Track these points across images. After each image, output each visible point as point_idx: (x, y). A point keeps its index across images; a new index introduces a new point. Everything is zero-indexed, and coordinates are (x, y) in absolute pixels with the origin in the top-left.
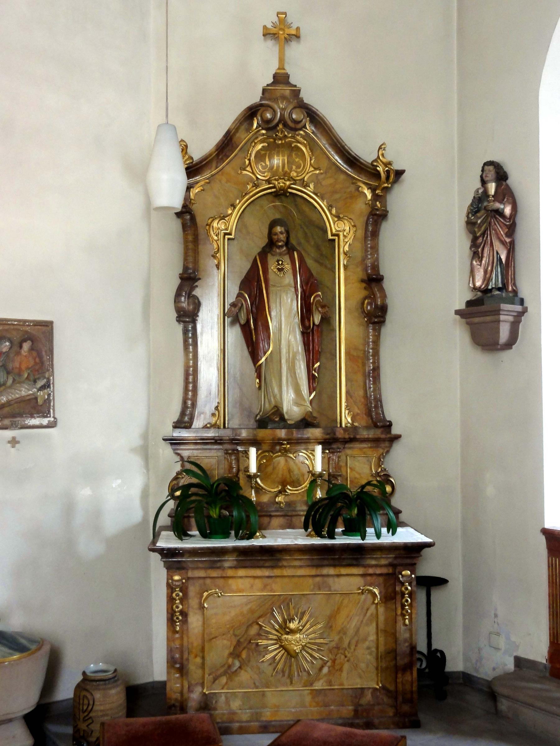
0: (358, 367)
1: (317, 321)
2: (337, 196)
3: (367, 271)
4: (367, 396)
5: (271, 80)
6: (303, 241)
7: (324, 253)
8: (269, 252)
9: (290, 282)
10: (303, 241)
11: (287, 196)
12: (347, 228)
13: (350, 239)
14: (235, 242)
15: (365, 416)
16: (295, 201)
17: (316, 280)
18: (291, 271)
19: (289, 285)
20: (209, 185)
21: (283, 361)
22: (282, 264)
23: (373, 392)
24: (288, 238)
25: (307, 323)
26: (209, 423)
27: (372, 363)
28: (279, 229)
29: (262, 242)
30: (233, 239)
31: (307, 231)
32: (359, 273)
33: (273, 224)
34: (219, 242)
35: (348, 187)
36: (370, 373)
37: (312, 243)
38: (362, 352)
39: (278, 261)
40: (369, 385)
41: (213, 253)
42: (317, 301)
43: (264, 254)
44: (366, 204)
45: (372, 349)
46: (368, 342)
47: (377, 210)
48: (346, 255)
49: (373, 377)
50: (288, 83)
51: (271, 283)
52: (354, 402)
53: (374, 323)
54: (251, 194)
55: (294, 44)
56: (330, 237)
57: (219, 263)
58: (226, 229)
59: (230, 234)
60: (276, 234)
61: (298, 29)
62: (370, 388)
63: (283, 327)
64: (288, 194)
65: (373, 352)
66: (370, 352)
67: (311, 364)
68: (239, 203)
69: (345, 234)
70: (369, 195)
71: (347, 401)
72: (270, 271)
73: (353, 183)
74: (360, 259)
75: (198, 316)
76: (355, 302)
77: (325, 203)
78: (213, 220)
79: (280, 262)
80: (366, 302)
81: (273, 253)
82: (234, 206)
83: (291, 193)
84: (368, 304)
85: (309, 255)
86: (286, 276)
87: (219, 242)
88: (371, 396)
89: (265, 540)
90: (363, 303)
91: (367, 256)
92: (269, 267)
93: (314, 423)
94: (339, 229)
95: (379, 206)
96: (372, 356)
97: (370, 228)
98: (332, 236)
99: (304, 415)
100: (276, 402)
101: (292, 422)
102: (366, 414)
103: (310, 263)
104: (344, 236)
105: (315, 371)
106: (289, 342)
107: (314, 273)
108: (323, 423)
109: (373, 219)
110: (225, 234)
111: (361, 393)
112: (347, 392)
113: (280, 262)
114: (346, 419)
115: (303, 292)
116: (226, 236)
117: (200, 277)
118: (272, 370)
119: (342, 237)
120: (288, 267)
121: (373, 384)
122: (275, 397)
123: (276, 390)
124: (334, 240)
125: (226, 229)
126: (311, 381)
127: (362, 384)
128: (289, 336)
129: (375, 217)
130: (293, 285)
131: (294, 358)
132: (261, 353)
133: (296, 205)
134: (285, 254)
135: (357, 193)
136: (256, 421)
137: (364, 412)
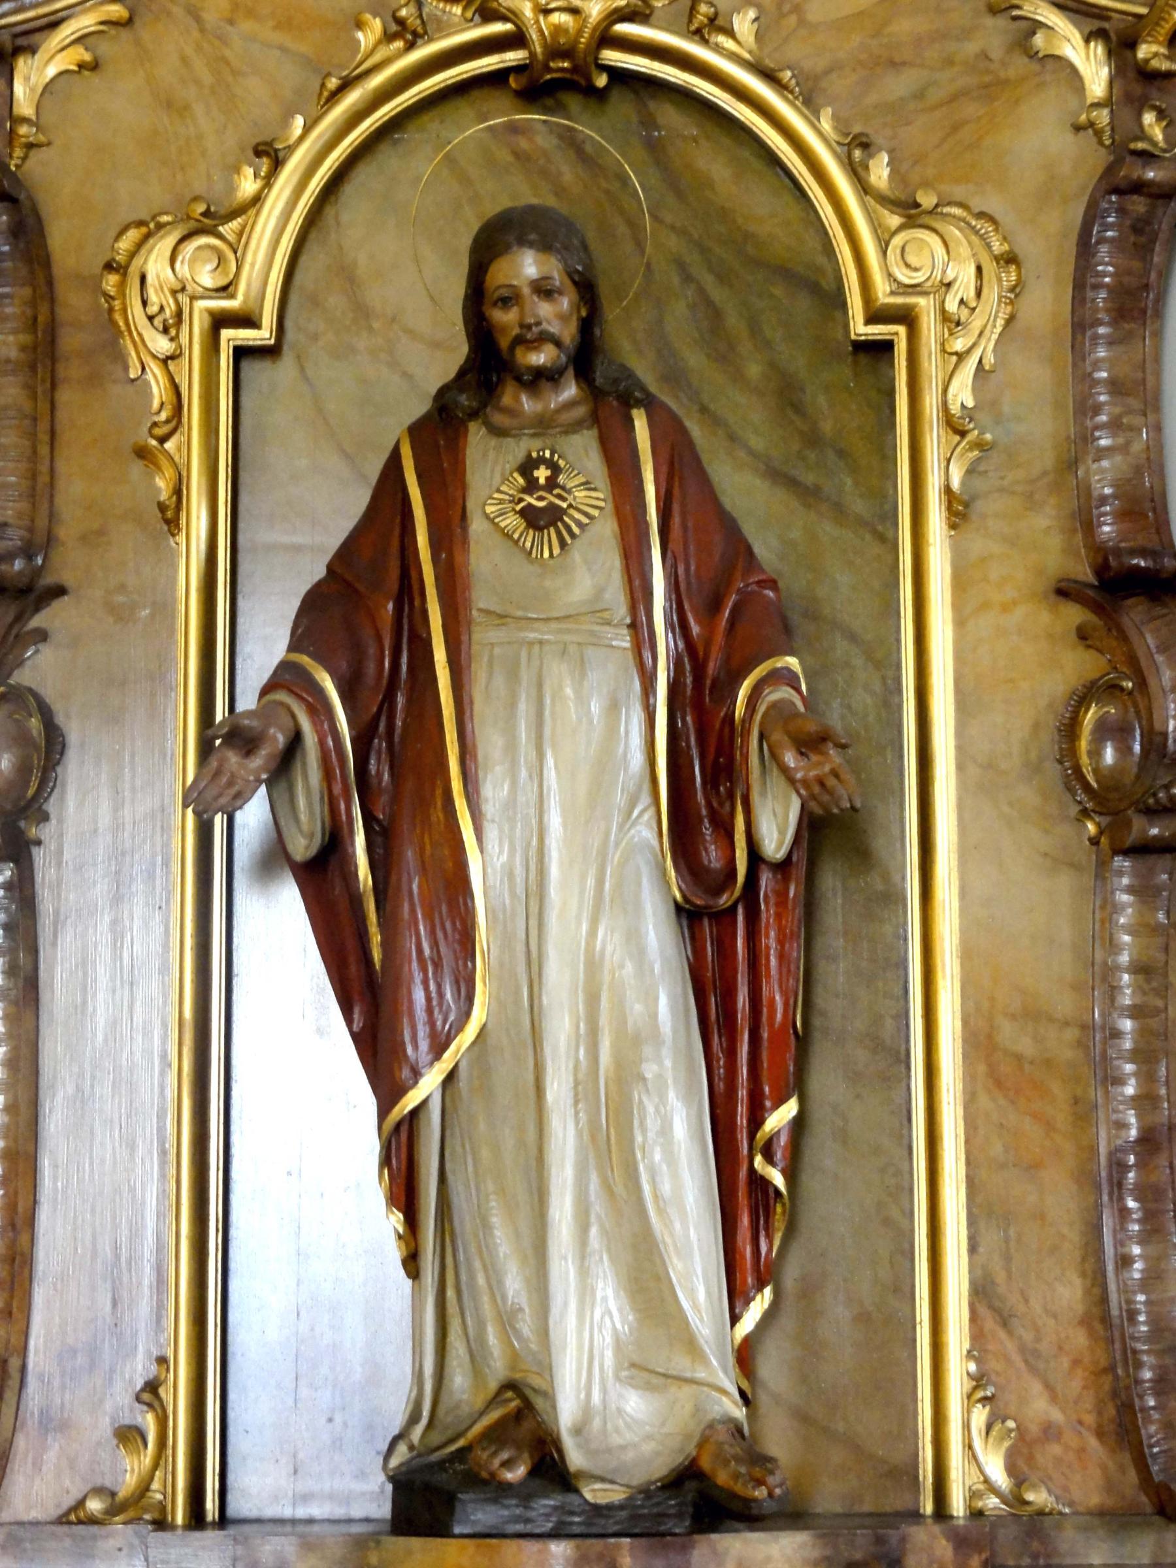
0: (1049, 1126)
1: (775, 838)
2: (898, 86)
3: (1089, 527)
4: (1106, 1319)
6: (694, 359)
7: (827, 427)
8: (474, 414)
9: (600, 591)
10: (694, 359)
11: (591, 92)
12: (964, 276)
13: (982, 336)
14: (285, 370)
15: (1093, 1442)
16: (649, 122)
17: (772, 584)
18: (606, 529)
19: (597, 612)
20: (124, 34)
21: (558, 1090)
22: (552, 484)
23: (1145, 1284)
24: (588, 326)
25: (713, 856)
26: (99, 1491)
27: (1136, 1101)
28: (528, 266)
29: (440, 357)
30: (269, 352)
31: (717, 294)
32: (1045, 544)
33: (489, 245)
34: (180, 370)
35: (966, 34)
36: (1123, 1168)
37: (754, 370)
38: (1071, 1034)
39: (527, 467)
40: (1119, 1243)
42: (774, 706)
43: (441, 431)
44: (1078, 128)
45: (1136, 1012)
46: (1108, 974)
47: (1147, 157)
48: (963, 434)
49: (1140, 1193)
51: (482, 598)
52: (1022, 1349)
53: (1142, 850)
54: (376, 81)
56: (861, 329)
57: (178, 492)
58: (225, 290)
59: (247, 321)
60: (508, 300)
62: (1125, 1261)
63: (554, 871)
64: (602, 81)
65: (1142, 1033)
66: (1116, 1034)
67: (742, 1110)
68: (301, 139)
69: (952, 306)
70: (1094, 71)
71: (978, 1348)
72: (477, 526)
74: (1048, 460)
75: (46, 818)
76: (1023, 718)
77: (826, 125)
78: (147, 237)
79: (542, 474)
80: (1090, 716)
81: (498, 419)
82: (271, 155)
83: (619, 76)
84: (1103, 731)
85: (732, 438)
86: (576, 554)
87: (180, 370)
88: (1132, 1315)
90: (1070, 730)
91: (1085, 438)
92: (471, 505)
93: (748, 1501)
94: (919, 278)
95: (1158, 134)
96: (1136, 1055)
97: (1106, 269)
98: (871, 320)
99: (691, 1449)
100: (514, 1358)
101: (613, 1495)
102: (1100, 1434)
103: (740, 488)
104: (945, 317)
105: (769, 1158)
106: (593, 965)
107: (765, 549)
108: (828, 1498)
109: (1121, 211)
110: (220, 321)
111: (1070, 1293)
112: (982, 1292)
113: (542, 474)
114: (976, 1466)
115: (691, 656)
116: (226, 334)
117: (67, 578)
118: (485, 1153)
119: (930, 326)
120: (586, 491)
121: (1144, 1239)
122: (507, 1320)
123: (514, 1285)
124: (885, 348)
125: (225, 290)
126: (745, 1220)
127: (1073, 1236)
128: (592, 933)
129: (1138, 205)
130: (621, 611)
131: (627, 1076)
132: (418, 1048)
133: (655, 148)
134: (574, 427)
135: (1019, 65)
136: (392, 1479)
137: (1090, 1419)
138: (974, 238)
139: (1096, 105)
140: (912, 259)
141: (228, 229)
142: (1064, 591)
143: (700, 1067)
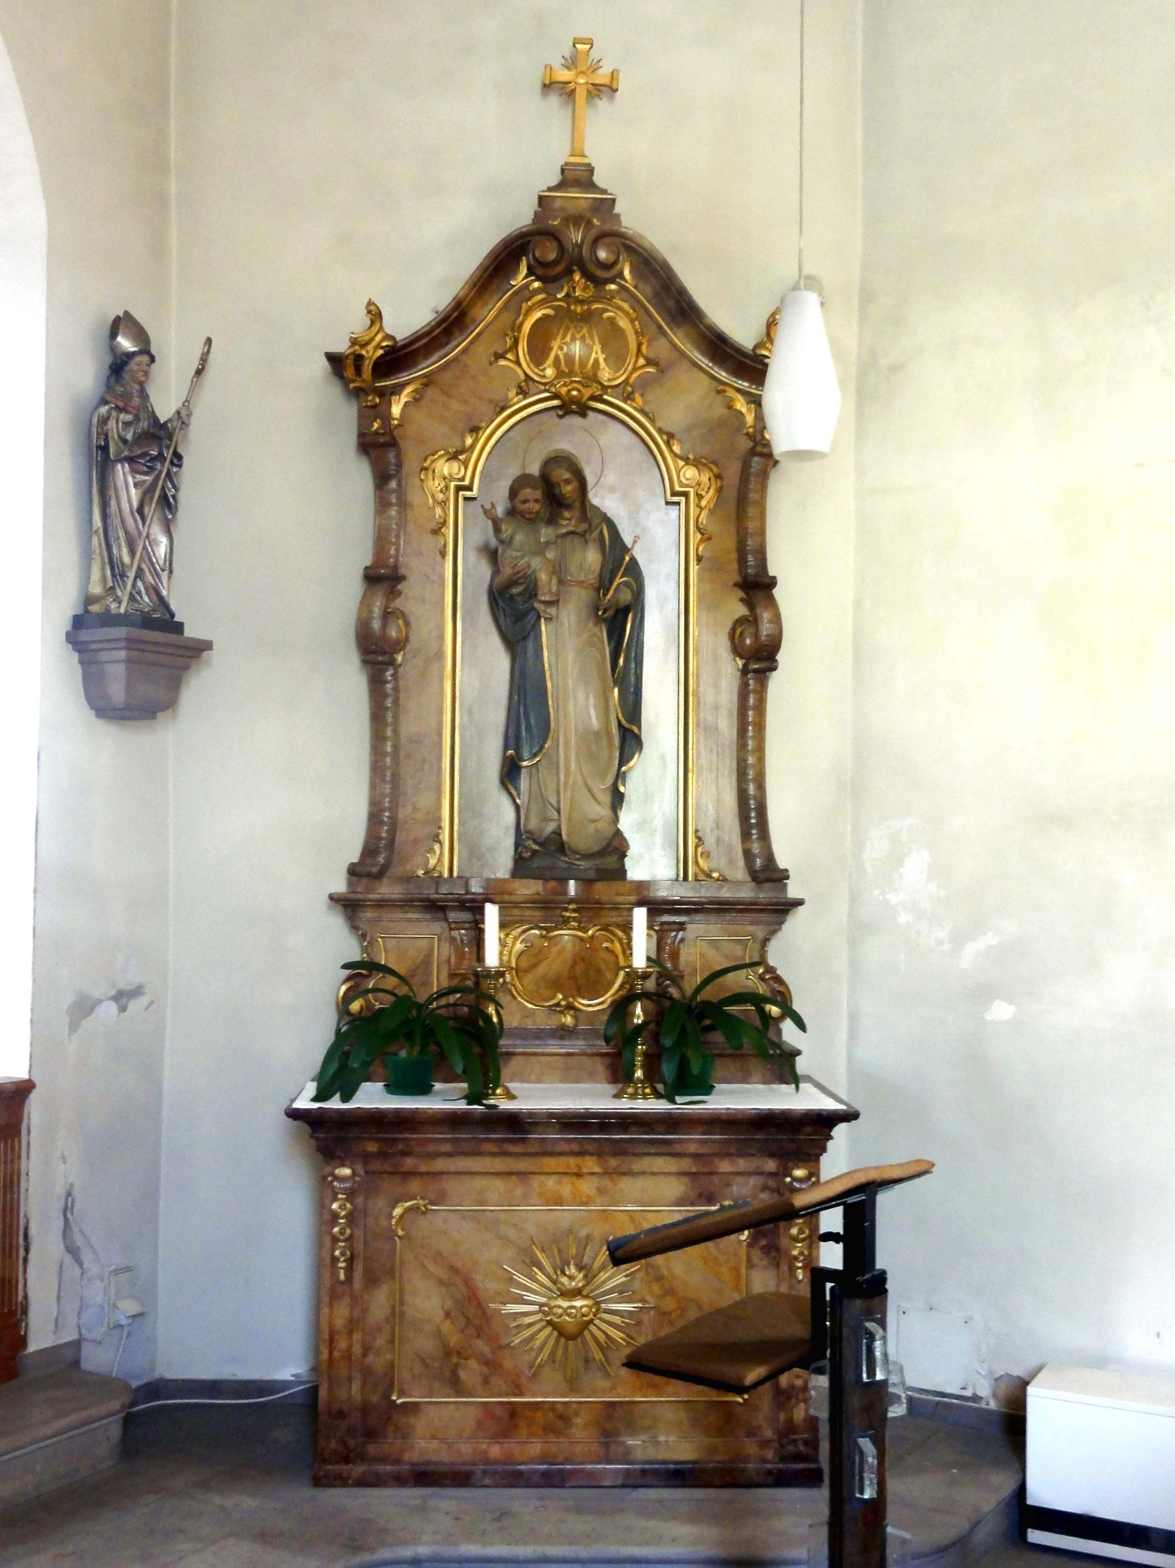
5: (554, 179)
12: (705, 477)
30: (473, 499)
41: (433, 525)
50: (590, 186)
55: (602, 104)
58: (463, 479)
59: (469, 488)
61: (614, 75)
73: (719, 392)
89: (515, 1101)
116: (461, 493)
141: (461, 457)
142: (736, 585)
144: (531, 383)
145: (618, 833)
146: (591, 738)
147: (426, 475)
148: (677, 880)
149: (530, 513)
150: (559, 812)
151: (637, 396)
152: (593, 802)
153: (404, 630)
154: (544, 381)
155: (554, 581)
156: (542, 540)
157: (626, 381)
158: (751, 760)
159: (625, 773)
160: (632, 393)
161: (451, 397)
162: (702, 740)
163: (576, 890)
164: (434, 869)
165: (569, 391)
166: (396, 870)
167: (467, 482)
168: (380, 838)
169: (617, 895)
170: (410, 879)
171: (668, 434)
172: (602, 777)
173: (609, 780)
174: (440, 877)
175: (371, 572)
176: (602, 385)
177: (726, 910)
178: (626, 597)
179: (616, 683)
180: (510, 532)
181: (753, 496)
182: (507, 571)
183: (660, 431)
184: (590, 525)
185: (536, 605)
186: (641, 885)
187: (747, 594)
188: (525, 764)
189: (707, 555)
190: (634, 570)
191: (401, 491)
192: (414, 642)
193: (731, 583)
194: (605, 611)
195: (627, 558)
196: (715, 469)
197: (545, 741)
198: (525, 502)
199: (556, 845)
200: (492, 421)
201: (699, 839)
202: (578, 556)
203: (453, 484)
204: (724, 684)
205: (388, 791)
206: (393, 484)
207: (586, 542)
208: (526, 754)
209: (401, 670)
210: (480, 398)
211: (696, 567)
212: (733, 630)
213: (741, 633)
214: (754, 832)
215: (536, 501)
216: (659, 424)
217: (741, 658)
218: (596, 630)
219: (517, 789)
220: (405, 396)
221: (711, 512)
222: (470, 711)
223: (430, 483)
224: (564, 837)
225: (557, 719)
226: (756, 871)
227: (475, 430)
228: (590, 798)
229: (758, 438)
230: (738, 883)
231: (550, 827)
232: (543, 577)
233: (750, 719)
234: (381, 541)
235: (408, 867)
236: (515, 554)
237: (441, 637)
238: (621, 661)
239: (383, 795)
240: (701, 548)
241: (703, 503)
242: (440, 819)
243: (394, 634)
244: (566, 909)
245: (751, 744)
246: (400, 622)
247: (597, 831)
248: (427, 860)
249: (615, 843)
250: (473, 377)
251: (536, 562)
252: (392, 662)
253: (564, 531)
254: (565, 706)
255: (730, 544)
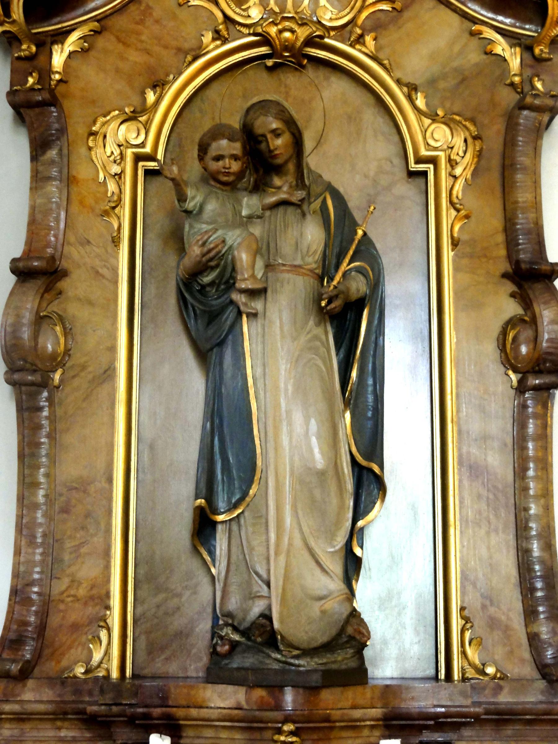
12: (458, 142)
56: (413, 167)
58: (142, 145)
59: (151, 158)
73: (473, 34)
110: (138, 158)
116: (141, 164)
124: (424, 174)
138: (448, 165)
139: (515, 75)
140: (436, 136)
141: (143, 119)
142: (505, 276)
143: (348, 520)
144: (231, 27)
145: (354, 614)
146: (313, 481)
147: (95, 140)
148: (436, 678)
149: (228, 174)
150: (268, 585)
151: (369, 39)
152: (318, 571)
153: (62, 340)
154: (249, 22)
155: (260, 264)
156: (244, 213)
157: (352, 22)
158: (533, 510)
159: (362, 529)
160: (362, 36)
161: (128, 46)
162: (466, 483)
163: (294, 701)
164: (99, 666)
165: (281, 32)
166: (49, 667)
167: (148, 149)
168: (26, 624)
169: (354, 707)
170: (63, 681)
171: (408, 85)
172: (331, 537)
173: (341, 540)
174: (107, 677)
175: (21, 265)
176: (323, 25)
177: (507, 721)
178: (358, 286)
179: (347, 403)
180: (199, 199)
181: (523, 160)
182: (195, 251)
183: (398, 82)
184: (309, 194)
185: (235, 296)
186: (389, 691)
187: (520, 286)
188: (220, 518)
189: (465, 237)
190: (366, 250)
191: (66, 159)
192: (77, 358)
193: (498, 273)
194: (329, 302)
195: (360, 232)
196: (472, 128)
197: (249, 487)
198: (218, 158)
199: (263, 634)
200: (180, 73)
201: (467, 620)
202: (292, 233)
203: (129, 153)
204: (493, 407)
205: (38, 558)
206: (52, 153)
207: (304, 215)
208: (222, 505)
209: (58, 395)
210: (166, 47)
211: (451, 254)
212: (504, 333)
213: (515, 339)
214: (541, 609)
215: (235, 157)
216: (398, 74)
217: (515, 371)
218: (319, 331)
219: (212, 553)
220: (72, 42)
221: (467, 184)
222: (152, 447)
223: (100, 150)
224: (276, 625)
225: (265, 454)
226: (546, 666)
227: (159, 85)
228: (313, 564)
229: (527, 88)
230: (520, 683)
231: (257, 608)
232: (244, 257)
233: (531, 453)
234: (36, 225)
235: (64, 663)
236: (205, 227)
237: (113, 349)
238: (354, 374)
239: (31, 563)
240: (457, 228)
241: (458, 171)
242: (108, 595)
243: (50, 347)
244: (279, 731)
245: (533, 487)
246: (58, 329)
247: (323, 612)
248: (90, 652)
249: (350, 630)
250: (157, 22)
251: (233, 237)
252: (45, 384)
253: (273, 199)
254: (277, 436)
255: (496, 223)
